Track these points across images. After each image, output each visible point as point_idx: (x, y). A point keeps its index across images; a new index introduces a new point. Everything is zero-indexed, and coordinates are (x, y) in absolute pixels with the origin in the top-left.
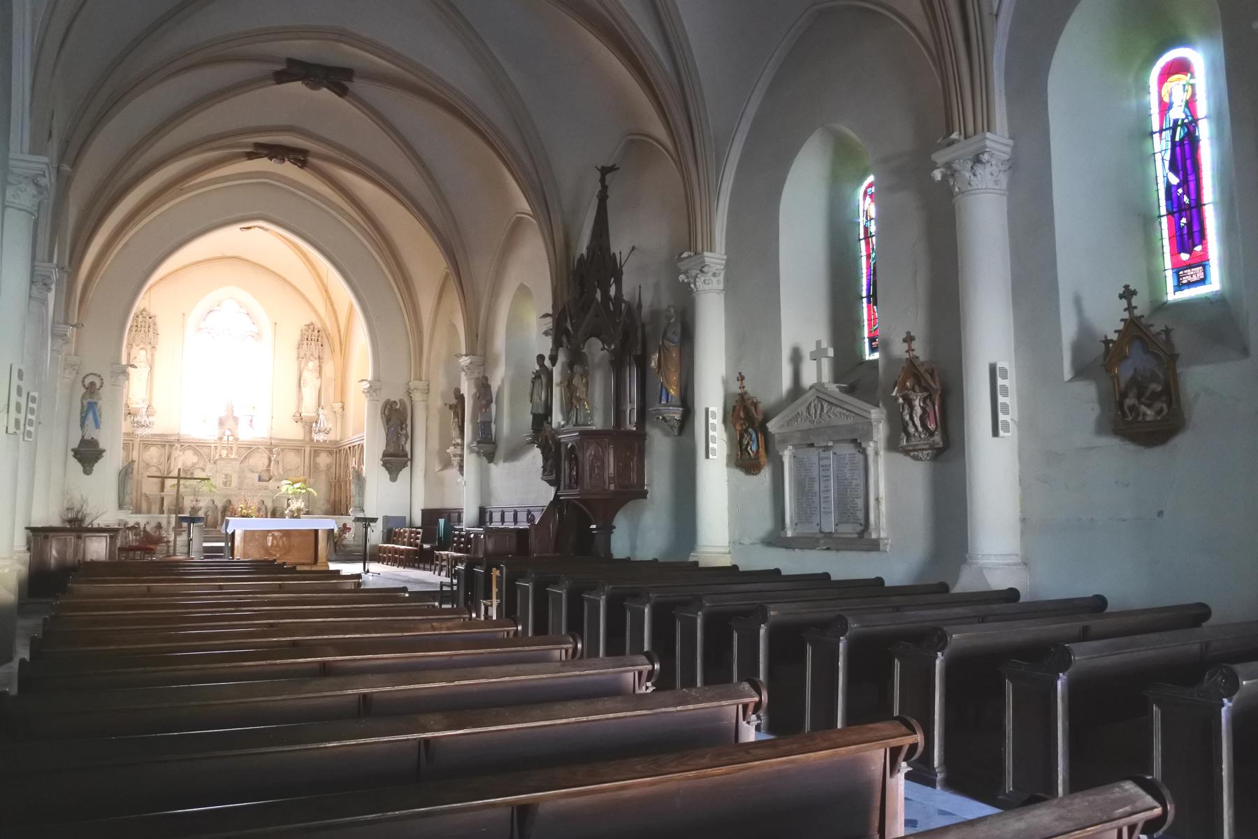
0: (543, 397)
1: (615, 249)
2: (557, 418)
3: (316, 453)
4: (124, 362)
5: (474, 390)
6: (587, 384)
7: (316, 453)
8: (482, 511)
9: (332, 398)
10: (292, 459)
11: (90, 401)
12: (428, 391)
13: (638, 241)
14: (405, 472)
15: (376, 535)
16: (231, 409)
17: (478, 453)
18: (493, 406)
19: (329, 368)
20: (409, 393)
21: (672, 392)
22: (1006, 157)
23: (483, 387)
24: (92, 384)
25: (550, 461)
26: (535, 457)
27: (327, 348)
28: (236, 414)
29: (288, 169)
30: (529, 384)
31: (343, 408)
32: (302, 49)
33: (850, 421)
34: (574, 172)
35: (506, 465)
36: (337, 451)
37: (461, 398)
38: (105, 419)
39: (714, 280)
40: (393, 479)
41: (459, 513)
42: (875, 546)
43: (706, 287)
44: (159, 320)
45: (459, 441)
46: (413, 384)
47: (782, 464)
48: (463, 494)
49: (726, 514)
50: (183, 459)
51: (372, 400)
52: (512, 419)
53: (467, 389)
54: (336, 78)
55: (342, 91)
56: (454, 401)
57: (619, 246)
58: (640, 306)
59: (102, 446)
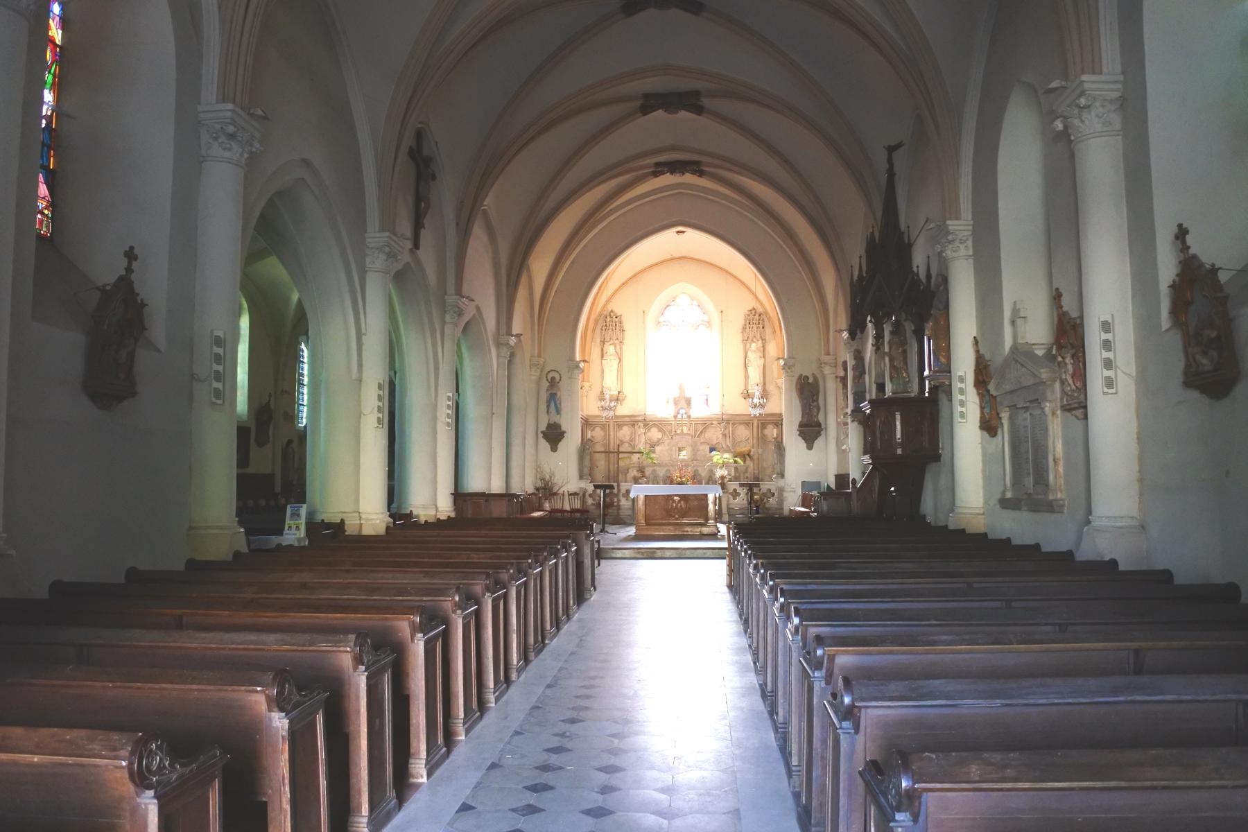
4: (578, 358)
9: (776, 375)
11: (553, 393)
14: (818, 443)
16: (681, 389)
22: (1116, 95)
24: (553, 378)
27: (768, 331)
28: (688, 395)
29: (689, 178)
32: (653, 84)
38: (565, 406)
39: (962, 246)
40: (810, 447)
42: (1051, 507)
43: (955, 255)
46: (825, 358)
49: (980, 476)
50: (655, 434)
51: (789, 376)
54: (689, 101)
55: (699, 110)
59: (563, 428)
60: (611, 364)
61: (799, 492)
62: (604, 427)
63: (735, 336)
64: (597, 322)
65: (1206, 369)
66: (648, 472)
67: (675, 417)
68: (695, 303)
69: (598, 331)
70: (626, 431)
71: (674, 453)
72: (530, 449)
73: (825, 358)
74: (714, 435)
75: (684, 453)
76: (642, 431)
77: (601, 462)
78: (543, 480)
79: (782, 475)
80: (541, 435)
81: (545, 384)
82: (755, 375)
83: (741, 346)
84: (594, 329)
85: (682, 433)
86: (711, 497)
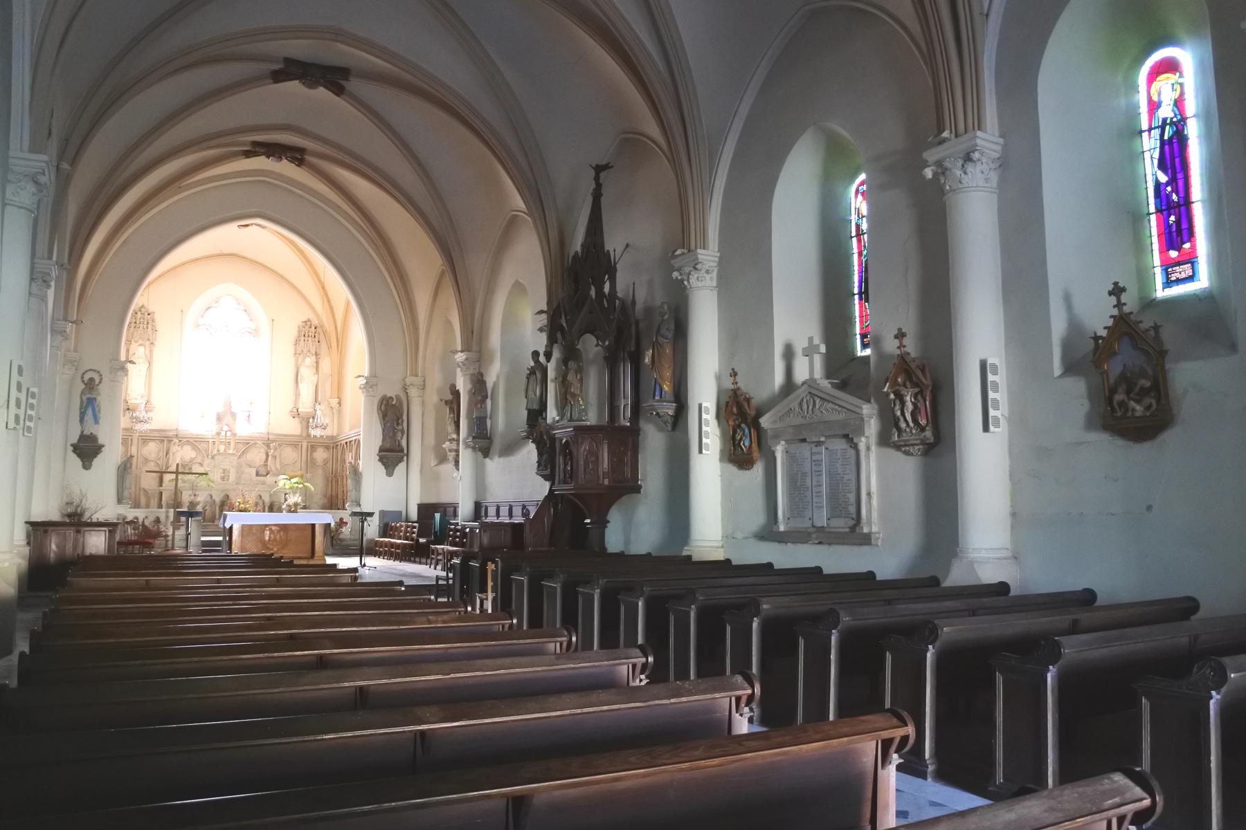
0: (538, 393)
1: (609, 246)
2: (552, 414)
3: (313, 448)
4: (123, 358)
5: (469, 386)
6: (581, 380)
7: (313, 448)
8: (478, 506)
9: (328, 394)
10: (289, 454)
11: (89, 396)
12: (423, 387)
13: (631, 239)
14: (401, 467)
15: (372, 529)
16: (229, 405)
17: (474, 448)
18: (489, 402)
19: (326, 364)
20: (405, 389)
21: (666, 388)
22: (997, 155)
23: (479, 383)
24: (92, 380)
25: (545, 456)
26: (530, 452)
27: (324, 345)
29: (285, 167)
30: (524, 380)
31: (340, 403)
32: (300, 49)
33: (842, 417)
34: (568, 170)
35: (502, 460)
36: (334, 446)
37: (456, 394)
39: (708, 277)
40: (390, 474)
41: (455, 507)
42: (866, 540)
43: (700, 284)
44: (157, 317)
45: (455, 436)
46: (409, 380)
47: (775, 459)
48: (458, 489)
49: (719, 509)
51: (369, 396)
52: (507, 414)
53: (462, 384)
54: (333, 77)
55: (339, 90)
56: (449, 397)
57: (613, 243)
58: (634, 302)
59: (101, 441)
65: (1137, 414)
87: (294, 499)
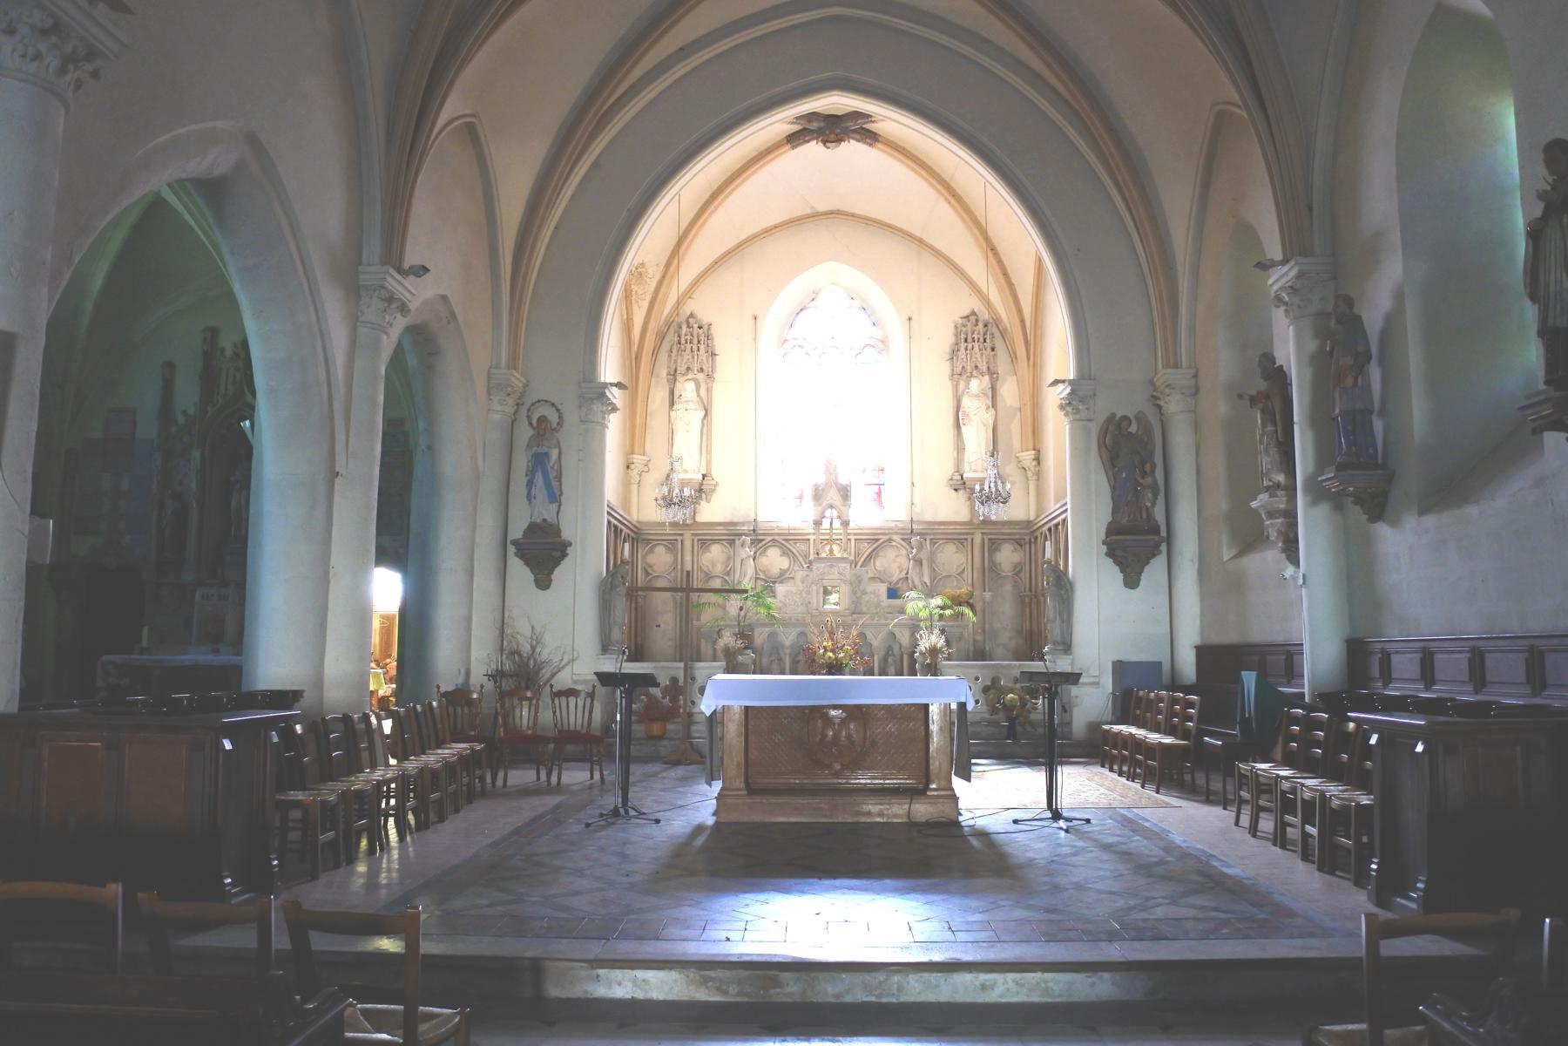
3: (993, 545)
7: (993, 545)
8: (1357, 651)
9: (1016, 443)
10: (951, 558)
12: (1196, 391)
14: (1155, 572)
15: (1091, 702)
16: (830, 470)
18: (1375, 372)
19: (1009, 391)
24: (542, 419)
28: (843, 481)
31: (1038, 460)
35: (1430, 521)
36: (1028, 536)
37: (1278, 378)
40: (1132, 582)
41: (1289, 655)
44: (715, 331)
45: (1281, 478)
46: (1164, 375)
48: (1305, 610)
50: (775, 560)
53: (1290, 347)
56: (1261, 385)
60: (687, 419)
61: (1108, 683)
62: (673, 546)
63: (937, 369)
64: (661, 336)
66: (760, 636)
67: (818, 523)
68: (856, 303)
69: (663, 356)
70: (716, 553)
71: (816, 600)
72: (485, 582)
73: (1164, 375)
74: (894, 562)
75: (834, 598)
76: (748, 551)
77: (664, 610)
78: (515, 653)
79: (1066, 647)
80: (511, 550)
81: (525, 433)
82: (976, 438)
83: (948, 386)
84: (655, 353)
85: (831, 558)
86: (934, 710)
87: (930, 640)
